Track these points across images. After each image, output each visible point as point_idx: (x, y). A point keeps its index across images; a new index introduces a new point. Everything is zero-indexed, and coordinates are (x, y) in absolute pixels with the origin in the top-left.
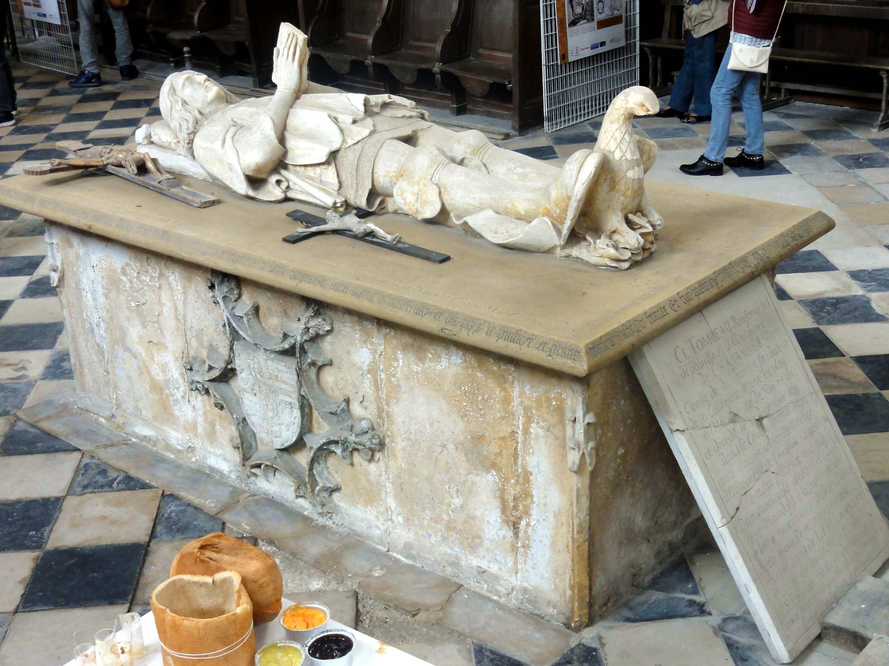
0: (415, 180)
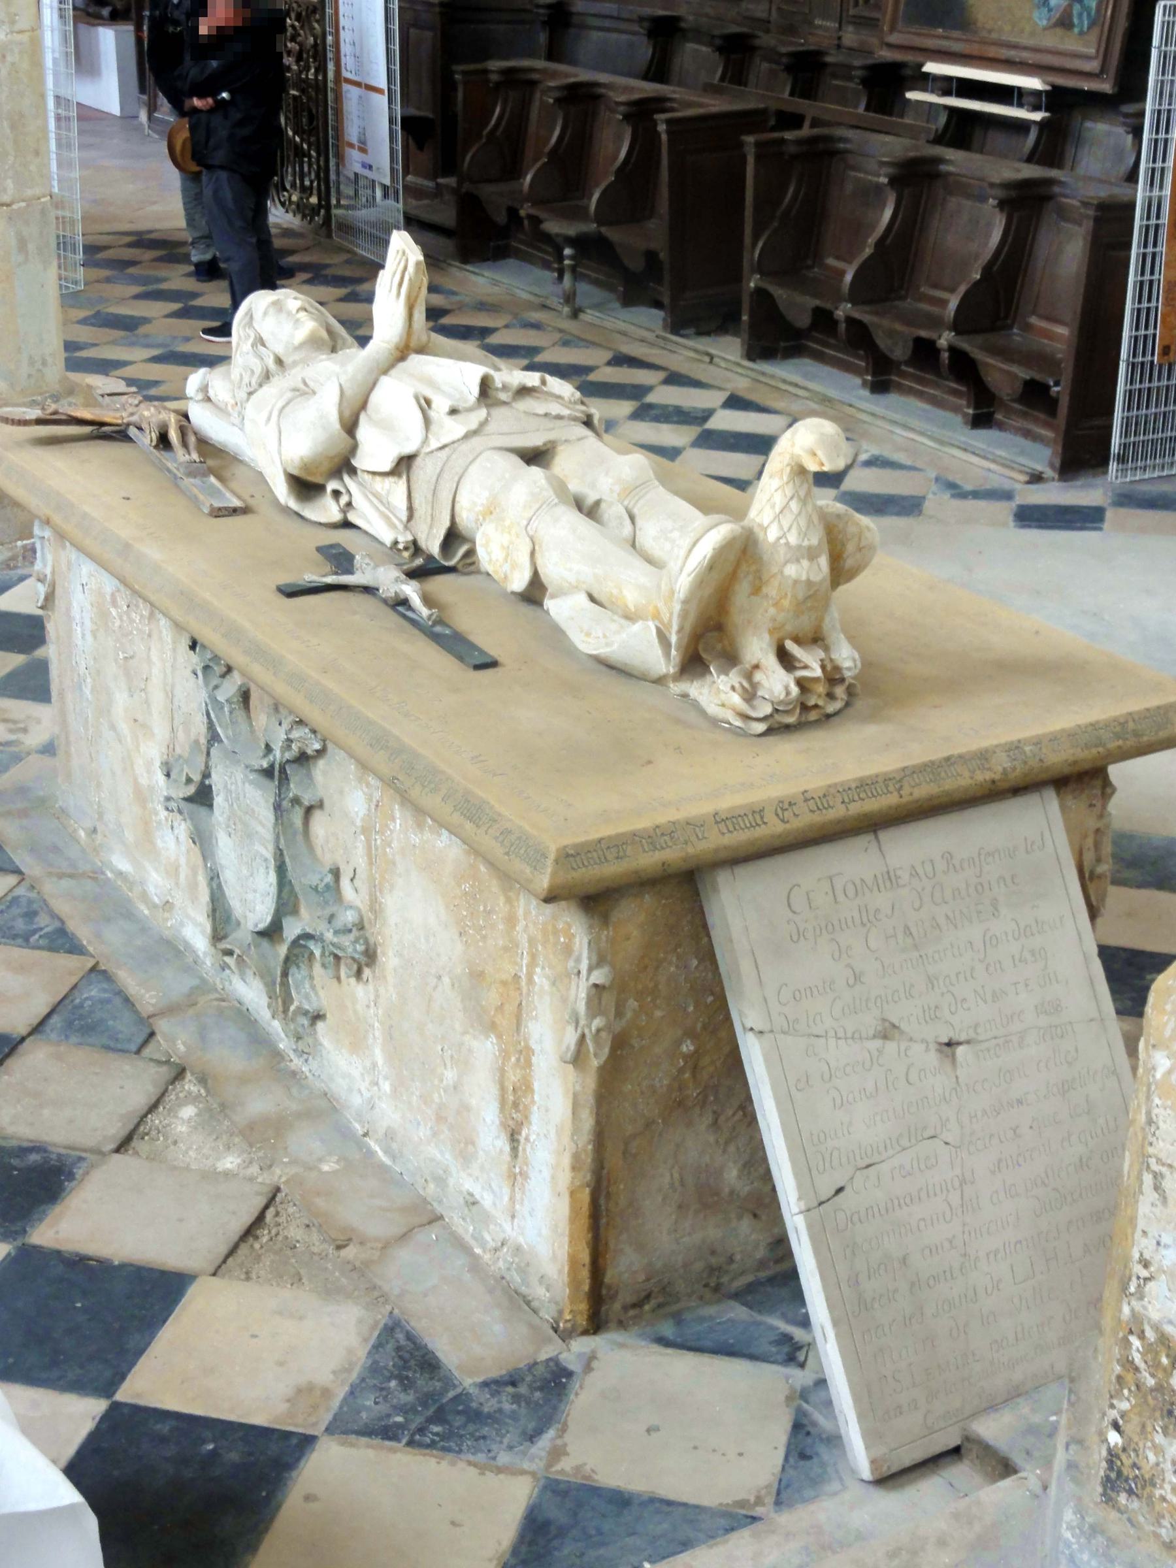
0: (507, 523)
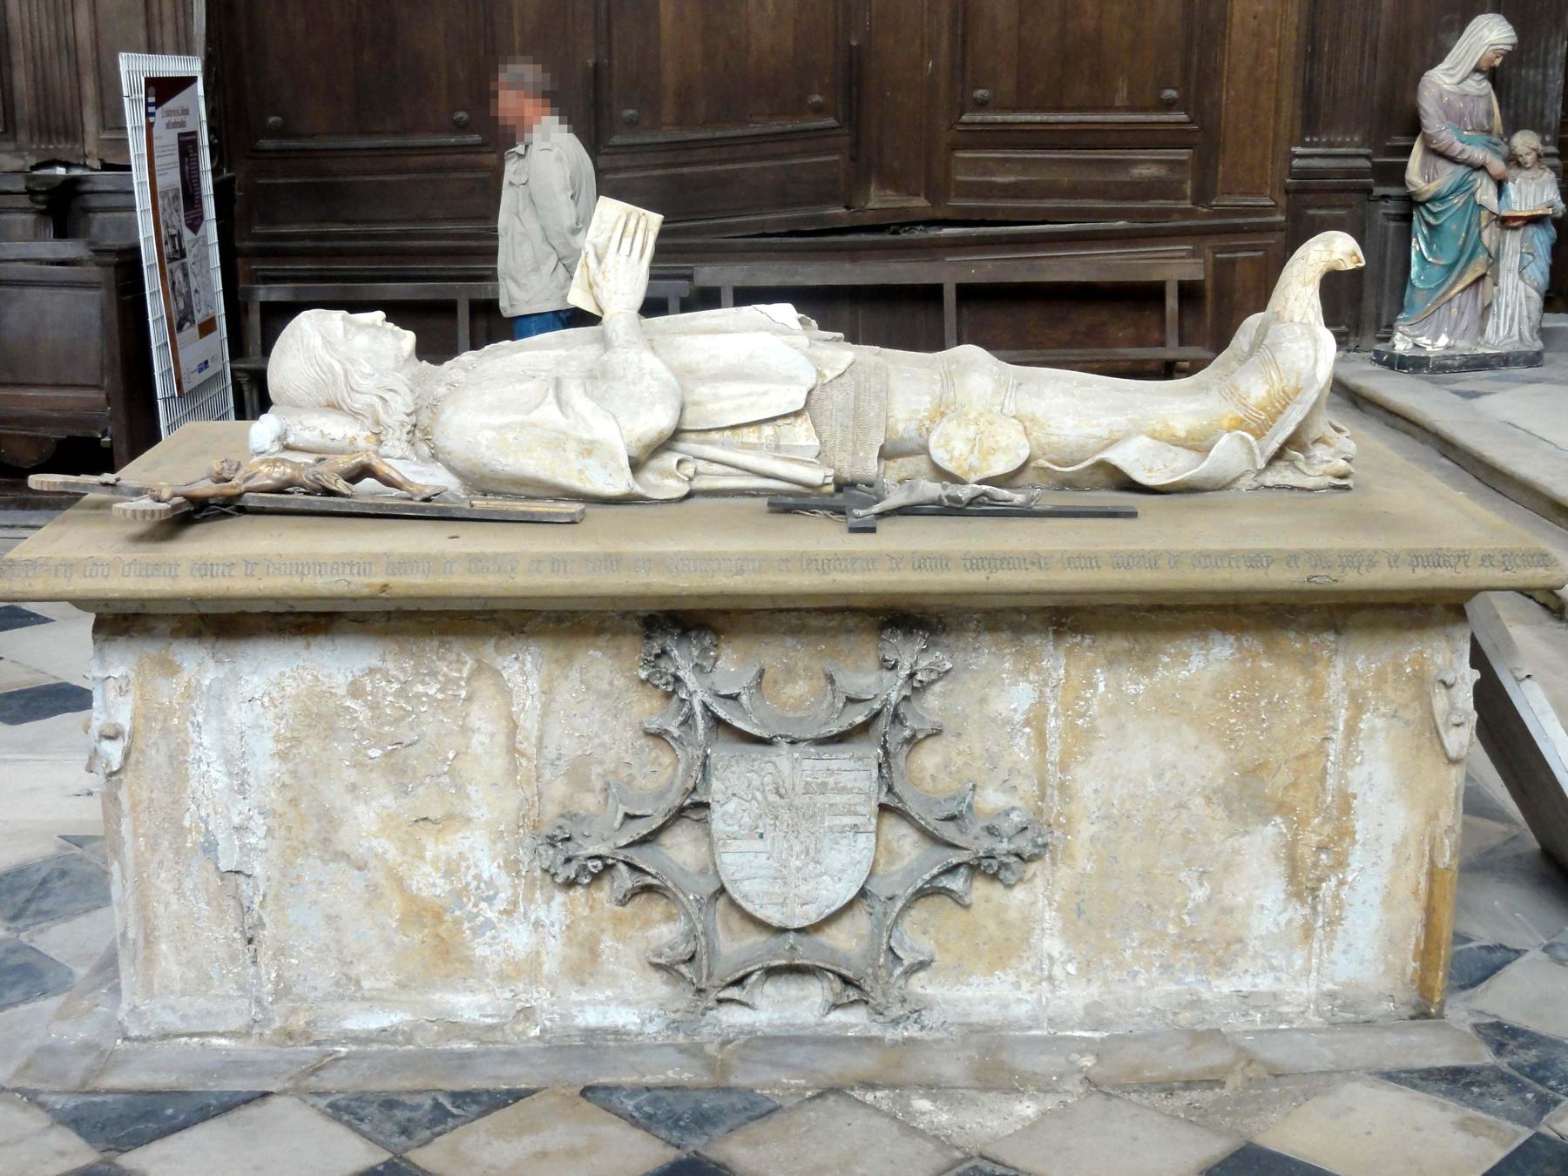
0: (972, 416)
